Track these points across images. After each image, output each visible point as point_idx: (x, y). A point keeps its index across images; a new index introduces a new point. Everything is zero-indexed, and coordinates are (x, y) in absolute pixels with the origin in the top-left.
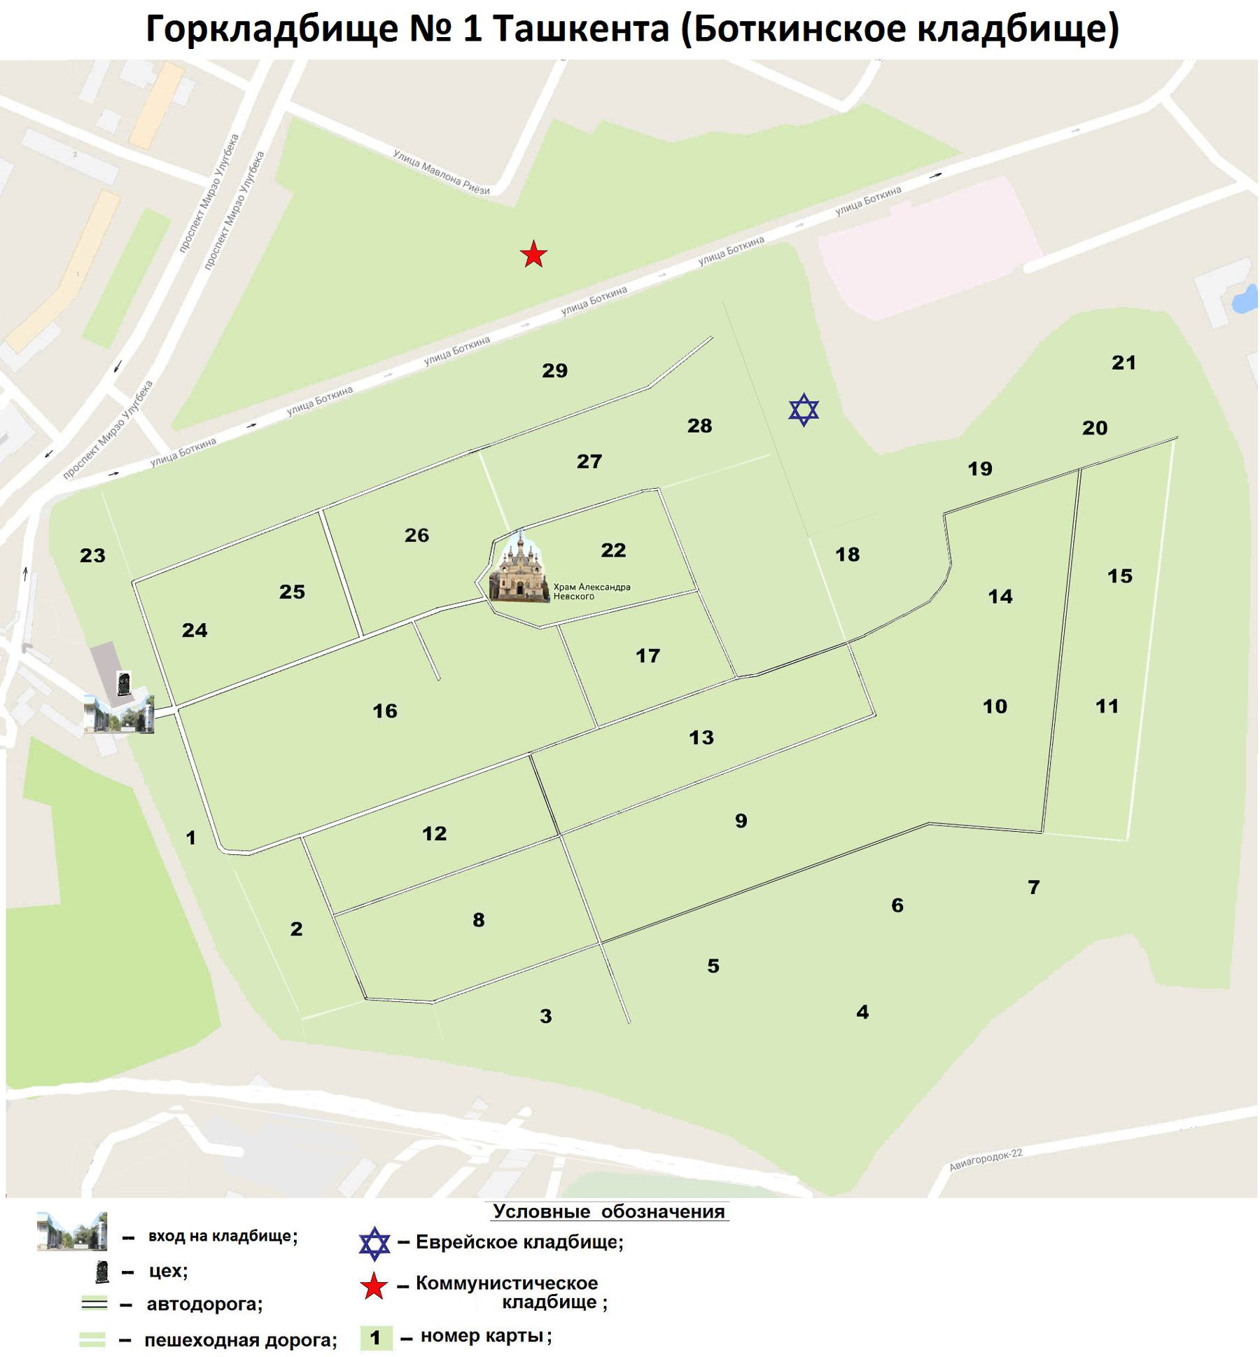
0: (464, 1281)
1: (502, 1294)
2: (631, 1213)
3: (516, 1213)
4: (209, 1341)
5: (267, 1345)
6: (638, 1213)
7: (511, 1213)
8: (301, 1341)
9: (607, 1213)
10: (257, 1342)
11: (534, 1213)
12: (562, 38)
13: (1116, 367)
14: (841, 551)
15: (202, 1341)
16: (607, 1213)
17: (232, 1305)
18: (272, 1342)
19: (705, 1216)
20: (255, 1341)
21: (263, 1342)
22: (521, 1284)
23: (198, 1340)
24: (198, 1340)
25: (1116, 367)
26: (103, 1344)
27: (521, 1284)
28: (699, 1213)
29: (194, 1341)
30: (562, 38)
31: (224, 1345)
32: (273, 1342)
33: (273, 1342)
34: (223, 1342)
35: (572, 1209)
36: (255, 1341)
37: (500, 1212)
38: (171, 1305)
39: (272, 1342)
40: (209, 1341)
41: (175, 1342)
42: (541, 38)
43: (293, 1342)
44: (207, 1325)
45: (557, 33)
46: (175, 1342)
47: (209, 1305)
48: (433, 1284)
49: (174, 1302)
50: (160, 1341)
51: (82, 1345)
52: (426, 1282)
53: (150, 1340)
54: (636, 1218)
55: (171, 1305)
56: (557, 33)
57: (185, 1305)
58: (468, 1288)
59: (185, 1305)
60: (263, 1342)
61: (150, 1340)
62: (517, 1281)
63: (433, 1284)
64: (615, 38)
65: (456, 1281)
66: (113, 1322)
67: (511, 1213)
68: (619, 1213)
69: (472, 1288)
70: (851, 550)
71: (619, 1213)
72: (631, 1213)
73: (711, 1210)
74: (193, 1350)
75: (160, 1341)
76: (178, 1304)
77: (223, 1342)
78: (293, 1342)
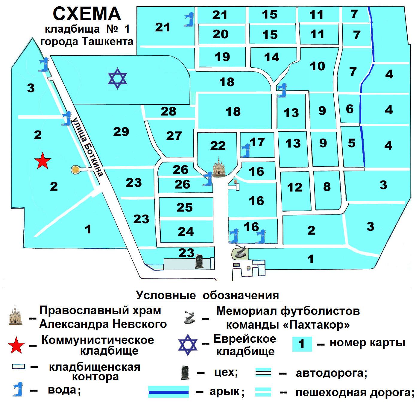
0: (71, 339)
1: (80, 346)
2: (221, 296)
3: (150, 296)
4: (335, 393)
5: (372, 396)
6: (225, 296)
7: (147, 296)
8: (392, 393)
9: (206, 296)
10: (365, 393)
11: (161, 296)
12: (102, 44)
13: (158, 30)
14: (229, 109)
15: (331, 393)
16: (206, 296)
17: (348, 374)
18: (374, 394)
19: (267, 298)
20: (364, 393)
21: (369, 393)
22: (106, 340)
23: (329, 393)
24: (329, 393)
25: (158, 30)
26: (269, 395)
27: (106, 340)
28: (263, 296)
29: (326, 393)
30: (102, 44)
31: (345, 395)
32: (375, 394)
33: (375, 394)
34: (344, 394)
35: (184, 294)
36: (364, 393)
37: (140, 296)
38: (310, 373)
39: (374, 394)
40: (335, 393)
41: (314, 394)
42: (96, 44)
43: (387, 394)
44: (333, 384)
45: (101, 43)
46: (314, 394)
47: (334, 374)
48: (52, 341)
49: (313, 372)
50: (305, 393)
51: (257, 395)
52: (48, 339)
53: (213, 392)
54: (224, 299)
55: (310, 373)
56: (101, 43)
57: (319, 374)
58: (74, 343)
59: (319, 374)
60: (369, 393)
61: (213, 392)
62: (104, 339)
63: (52, 341)
64: (117, 44)
65: (66, 339)
66: (276, 383)
67: (147, 296)
68: (214, 296)
69: (76, 343)
70: (235, 109)
71: (214, 296)
72: (221, 296)
73: (270, 294)
74: (326, 399)
75: (305, 393)
76: (315, 373)
77: (344, 394)
78: (387, 394)
